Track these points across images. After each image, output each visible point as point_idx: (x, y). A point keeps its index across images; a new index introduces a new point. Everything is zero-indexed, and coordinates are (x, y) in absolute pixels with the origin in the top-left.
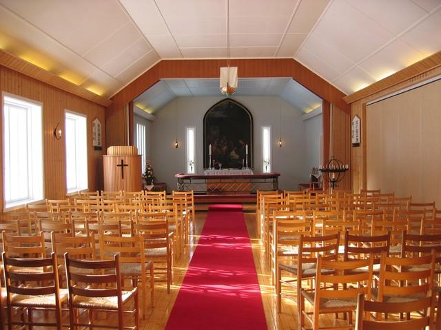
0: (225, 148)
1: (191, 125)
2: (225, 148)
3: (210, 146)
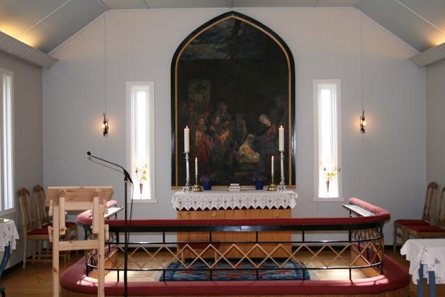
0: (225, 135)
1: (140, 78)
2: (225, 135)
3: (187, 131)
